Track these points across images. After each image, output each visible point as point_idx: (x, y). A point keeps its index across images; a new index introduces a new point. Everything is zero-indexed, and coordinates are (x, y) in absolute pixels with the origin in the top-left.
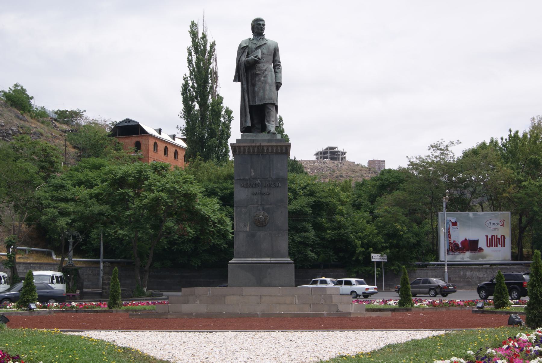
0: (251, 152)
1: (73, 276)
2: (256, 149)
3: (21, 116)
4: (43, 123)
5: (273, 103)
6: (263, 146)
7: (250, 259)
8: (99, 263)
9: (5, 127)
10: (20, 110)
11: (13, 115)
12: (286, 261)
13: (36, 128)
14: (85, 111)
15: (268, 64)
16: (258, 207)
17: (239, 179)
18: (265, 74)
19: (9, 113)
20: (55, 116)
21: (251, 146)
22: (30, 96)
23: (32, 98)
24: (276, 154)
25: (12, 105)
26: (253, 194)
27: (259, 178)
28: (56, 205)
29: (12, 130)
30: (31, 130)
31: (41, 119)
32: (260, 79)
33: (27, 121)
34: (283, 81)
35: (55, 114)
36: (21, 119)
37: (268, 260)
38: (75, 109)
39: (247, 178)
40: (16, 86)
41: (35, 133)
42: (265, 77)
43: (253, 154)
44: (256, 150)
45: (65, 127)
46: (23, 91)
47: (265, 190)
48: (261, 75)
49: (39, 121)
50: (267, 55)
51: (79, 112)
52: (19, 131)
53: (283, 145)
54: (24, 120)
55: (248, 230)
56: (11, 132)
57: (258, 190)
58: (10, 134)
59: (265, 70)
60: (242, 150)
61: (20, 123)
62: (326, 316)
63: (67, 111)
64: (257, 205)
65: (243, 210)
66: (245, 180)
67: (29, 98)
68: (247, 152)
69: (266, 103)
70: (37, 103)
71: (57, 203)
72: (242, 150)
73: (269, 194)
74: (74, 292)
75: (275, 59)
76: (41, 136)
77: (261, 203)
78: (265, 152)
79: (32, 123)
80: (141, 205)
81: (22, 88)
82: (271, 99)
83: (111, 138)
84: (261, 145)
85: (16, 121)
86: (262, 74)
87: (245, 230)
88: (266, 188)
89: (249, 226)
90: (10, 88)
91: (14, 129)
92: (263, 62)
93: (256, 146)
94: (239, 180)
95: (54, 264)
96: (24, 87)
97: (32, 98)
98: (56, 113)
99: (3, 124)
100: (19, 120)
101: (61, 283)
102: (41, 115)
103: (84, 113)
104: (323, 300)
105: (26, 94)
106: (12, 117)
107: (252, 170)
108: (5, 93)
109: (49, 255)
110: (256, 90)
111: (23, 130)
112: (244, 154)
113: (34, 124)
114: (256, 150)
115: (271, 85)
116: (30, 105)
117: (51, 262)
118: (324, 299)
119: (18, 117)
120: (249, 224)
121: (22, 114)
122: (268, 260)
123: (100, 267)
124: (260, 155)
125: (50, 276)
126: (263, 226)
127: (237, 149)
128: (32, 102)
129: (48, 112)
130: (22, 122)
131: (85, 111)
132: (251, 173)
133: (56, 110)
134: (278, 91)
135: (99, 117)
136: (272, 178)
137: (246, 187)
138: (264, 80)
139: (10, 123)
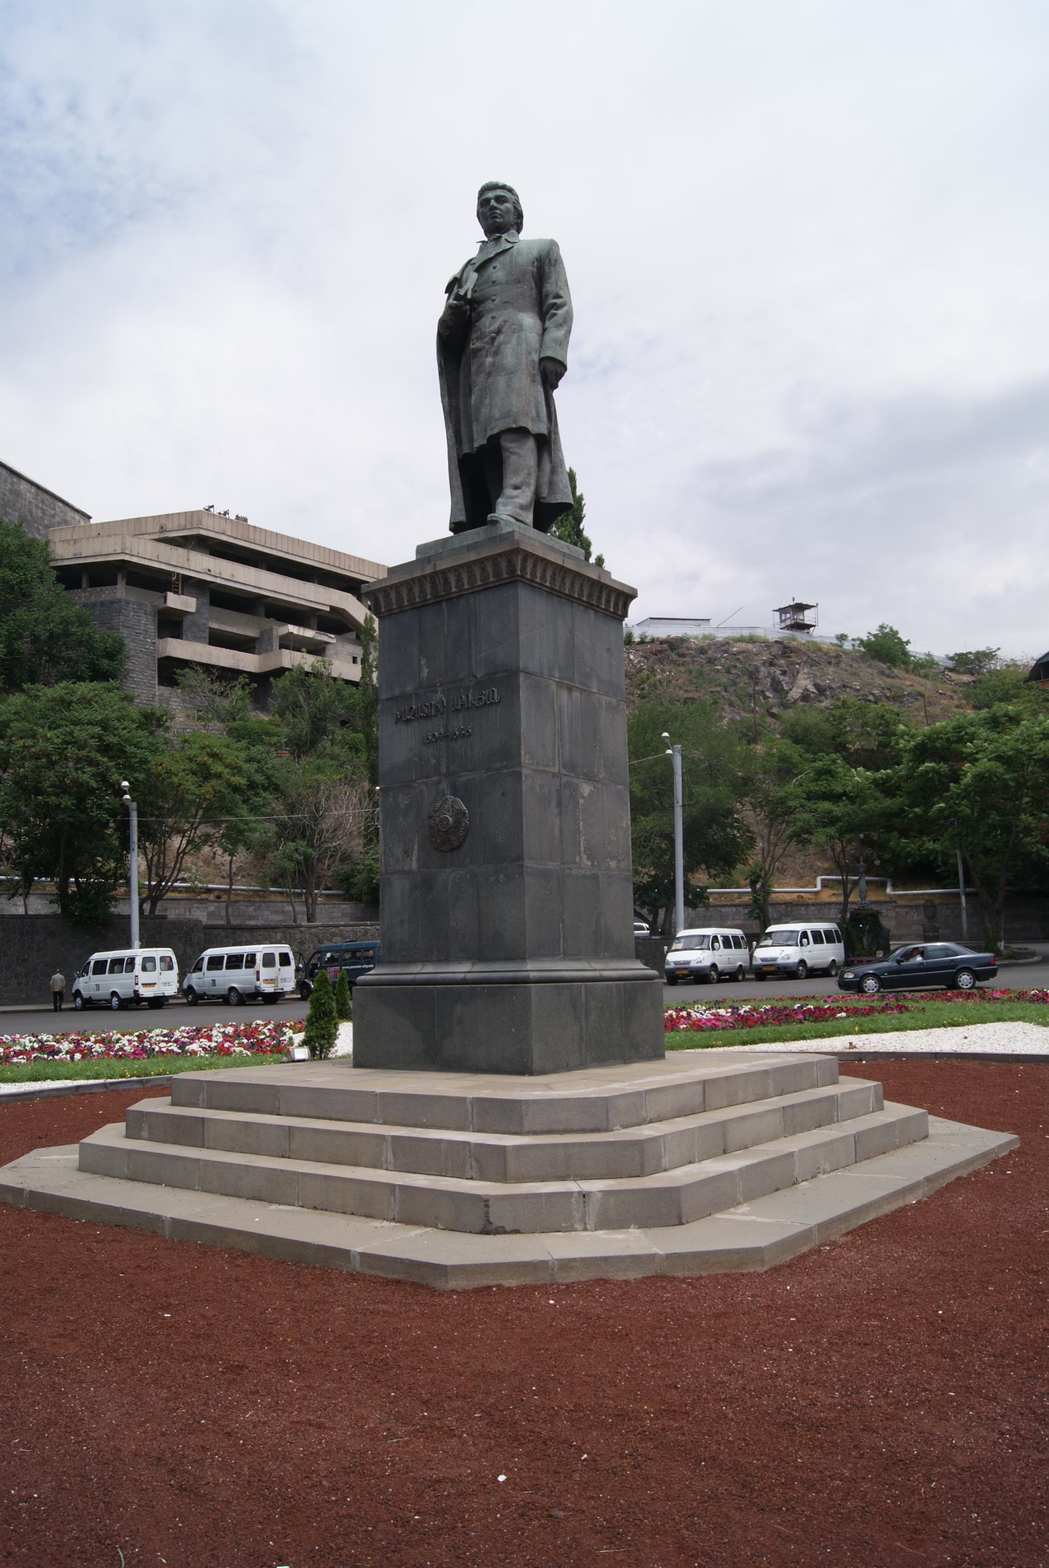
0: (417, 600)
1: (867, 927)
2: (428, 586)
3: (887, 672)
4: (926, 676)
5: (514, 426)
6: (443, 572)
7: (430, 968)
8: (957, 895)
9: (861, 692)
10: (884, 663)
11: (875, 672)
12: (511, 974)
13: (912, 686)
14: (999, 649)
15: (511, 310)
16: (439, 782)
17: (389, 697)
18: (496, 344)
19: (869, 670)
20: (950, 664)
21: (413, 580)
22: (904, 639)
23: (908, 642)
24: (487, 588)
25: (873, 658)
26: (427, 742)
27: (441, 685)
28: (814, 807)
29: (873, 694)
30: (904, 690)
31: (922, 672)
32: (481, 366)
33: (899, 678)
34: (571, 359)
35: (950, 662)
36: (888, 676)
37: (461, 970)
38: (982, 648)
39: (409, 689)
40: (882, 627)
41: (910, 694)
42: (496, 353)
43: (424, 605)
44: (428, 592)
45: (966, 678)
46: (894, 634)
47: (458, 723)
48: (484, 352)
49: (919, 675)
50: (507, 283)
51: (991, 653)
52: (885, 695)
53: (498, 551)
54: (892, 677)
55: (414, 866)
56: (871, 698)
57: (436, 726)
58: (870, 701)
59: (499, 332)
60: (394, 600)
61: (886, 682)
62: (358, 1268)
63: (970, 653)
64: (435, 778)
65: (400, 800)
66: (405, 697)
67: (902, 644)
68: (406, 603)
69: (496, 431)
70: (917, 648)
71: (816, 803)
72: (394, 600)
73: (466, 735)
74: (872, 955)
75: (544, 290)
76: (919, 698)
77: (448, 768)
78: (454, 590)
79: (906, 679)
80: (959, 791)
81: (891, 629)
82: (507, 414)
83: (1030, 683)
84: (438, 569)
85: (879, 681)
86: (487, 347)
87: (406, 868)
88: (461, 715)
89: (415, 852)
90: (869, 633)
91: (876, 692)
92: (490, 311)
93: (425, 576)
94: (392, 699)
95: (885, 902)
96: (895, 629)
97: (908, 642)
98: (951, 659)
99: (858, 687)
100: (884, 678)
101: (827, 942)
102: (926, 667)
103: (998, 653)
104: (474, 1164)
105: (899, 639)
106: (872, 674)
107: (423, 662)
108: (862, 641)
109: (883, 886)
110: (473, 402)
111: (891, 691)
112: (402, 611)
113: (910, 681)
114: (428, 592)
115: (512, 373)
116: (906, 654)
117: (882, 898)
118: (477, 1161)
119: (882, 673)
120: (416, 847)
121: (889, 668)
122: (461, 970)
123: (960, 903)
124: (444, 604)
125: (798, 932)
126: (452, 850)
127: (381, 599)
128: (909, 648)
129: (936, 659)
130: (889, 681)
131: (999, 649)
132: (420, 670)
133: (951, 655)
134: (556, 394)
135: (1023, 654)
136: (476, 677)
137: (408, 721)
138: (493, 365)
139: (869, 684)
